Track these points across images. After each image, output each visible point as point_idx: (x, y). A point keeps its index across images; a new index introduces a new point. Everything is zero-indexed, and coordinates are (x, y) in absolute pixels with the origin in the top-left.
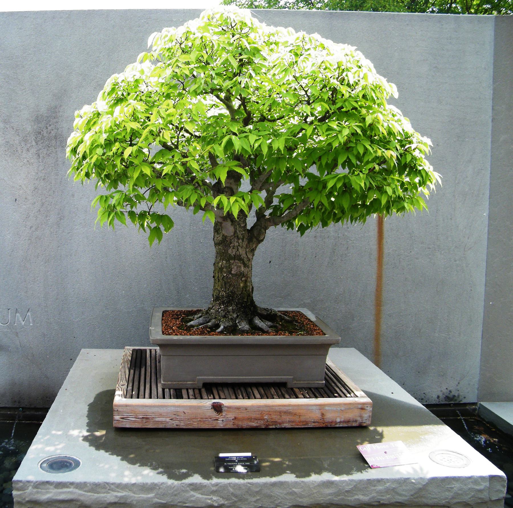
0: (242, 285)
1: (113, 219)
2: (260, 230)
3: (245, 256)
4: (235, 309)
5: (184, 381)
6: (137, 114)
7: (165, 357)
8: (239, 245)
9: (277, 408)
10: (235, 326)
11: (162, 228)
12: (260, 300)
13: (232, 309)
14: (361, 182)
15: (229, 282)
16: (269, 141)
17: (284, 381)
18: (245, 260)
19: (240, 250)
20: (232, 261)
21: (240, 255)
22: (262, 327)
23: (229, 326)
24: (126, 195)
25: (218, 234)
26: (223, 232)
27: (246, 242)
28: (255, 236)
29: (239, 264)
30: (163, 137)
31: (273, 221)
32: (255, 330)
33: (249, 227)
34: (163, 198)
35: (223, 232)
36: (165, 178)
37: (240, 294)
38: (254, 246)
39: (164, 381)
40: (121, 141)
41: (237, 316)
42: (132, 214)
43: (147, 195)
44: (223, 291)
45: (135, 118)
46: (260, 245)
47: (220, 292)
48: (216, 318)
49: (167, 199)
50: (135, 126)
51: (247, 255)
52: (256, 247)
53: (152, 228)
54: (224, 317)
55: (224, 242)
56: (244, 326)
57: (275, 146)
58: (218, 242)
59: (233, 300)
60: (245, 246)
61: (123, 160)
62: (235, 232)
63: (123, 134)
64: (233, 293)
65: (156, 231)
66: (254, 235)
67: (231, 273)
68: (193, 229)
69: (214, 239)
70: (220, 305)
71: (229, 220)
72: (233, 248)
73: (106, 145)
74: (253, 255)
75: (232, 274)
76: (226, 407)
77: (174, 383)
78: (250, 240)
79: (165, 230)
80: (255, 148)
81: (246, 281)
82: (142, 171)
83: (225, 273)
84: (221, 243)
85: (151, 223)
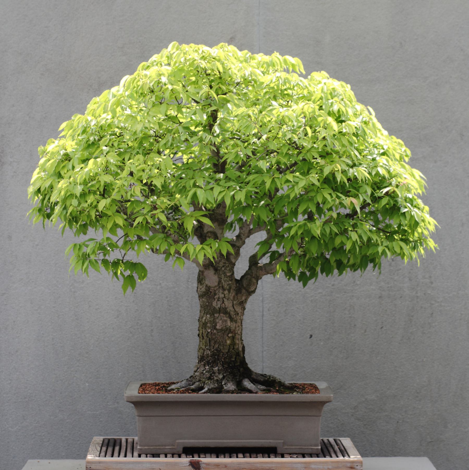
0: (228, 342)
1: (87, 267)
2: (250, 280)
3: (232, 308)
4: (221, 370)
5: (162, 446)
6: (110, 166)
7: (141, 418)
8: (225, 297)
9: (258, 465)
10: (222, 387)
11: (135, 276)
12: (257, 362)
13: (218, 370)
14: (318, 229)
15: (213, 339)
16: (232, 193)
17: (273, 445)
18: (232, 313)
19: (226, 302)
20: (216, 315)
21: (226, 308)
22: (251, 389)
23: (214, 388)
24: (100, 244)
25: (201, 284)
26: (207, 282)
27: (234, 294)
28: (245, 287)
29: (225, 318)
30: (134, 192)
31: (265, 269)
32: (241, 389)
33: (238, 276)
34: (136, 248)
35: (207, 282)
36: (137, 227)
37: (227, 353)
38: (243, 298)
39: (140, 446)
40: (95, 193)
41: (224, 377)
42: (105, 262)
43: (120, 243)
44: (207, 349)
45: (107, 170)
46: (251, 298)
47: (204, 350)
48: (200, 381)
49: (139, 247)
50: (108, 179)
51: (234, 308)
52: (246, 300)
53: (126, 276)
54: (209, 378)
55: (208, 293)
56: (231, 386)
57: (237, 198)
58: (202, 293)
59: (218, 359)
60: (232, 298)
61: (97, 211)
62: (220, 282)
63: (97, 187)
64: (219, 351)
65: (130, 280)
66: (243, 285)
67: (215, 328)
68: (174, 278)
69: (197, 290)
70: (204, 365)
71: (211, 269)
72: (218, 300)
73: (81, 195)
74: (244, 309)
75: (216, 329)
76: (204, 463)
77: (152, 448)
78: (238, 291)
79: (139, 278)
80: (218, 200)
81: (233, 338)
82: (115, 222)
83: (209, 328)
84: (205, 295)
85: (125, 271)
